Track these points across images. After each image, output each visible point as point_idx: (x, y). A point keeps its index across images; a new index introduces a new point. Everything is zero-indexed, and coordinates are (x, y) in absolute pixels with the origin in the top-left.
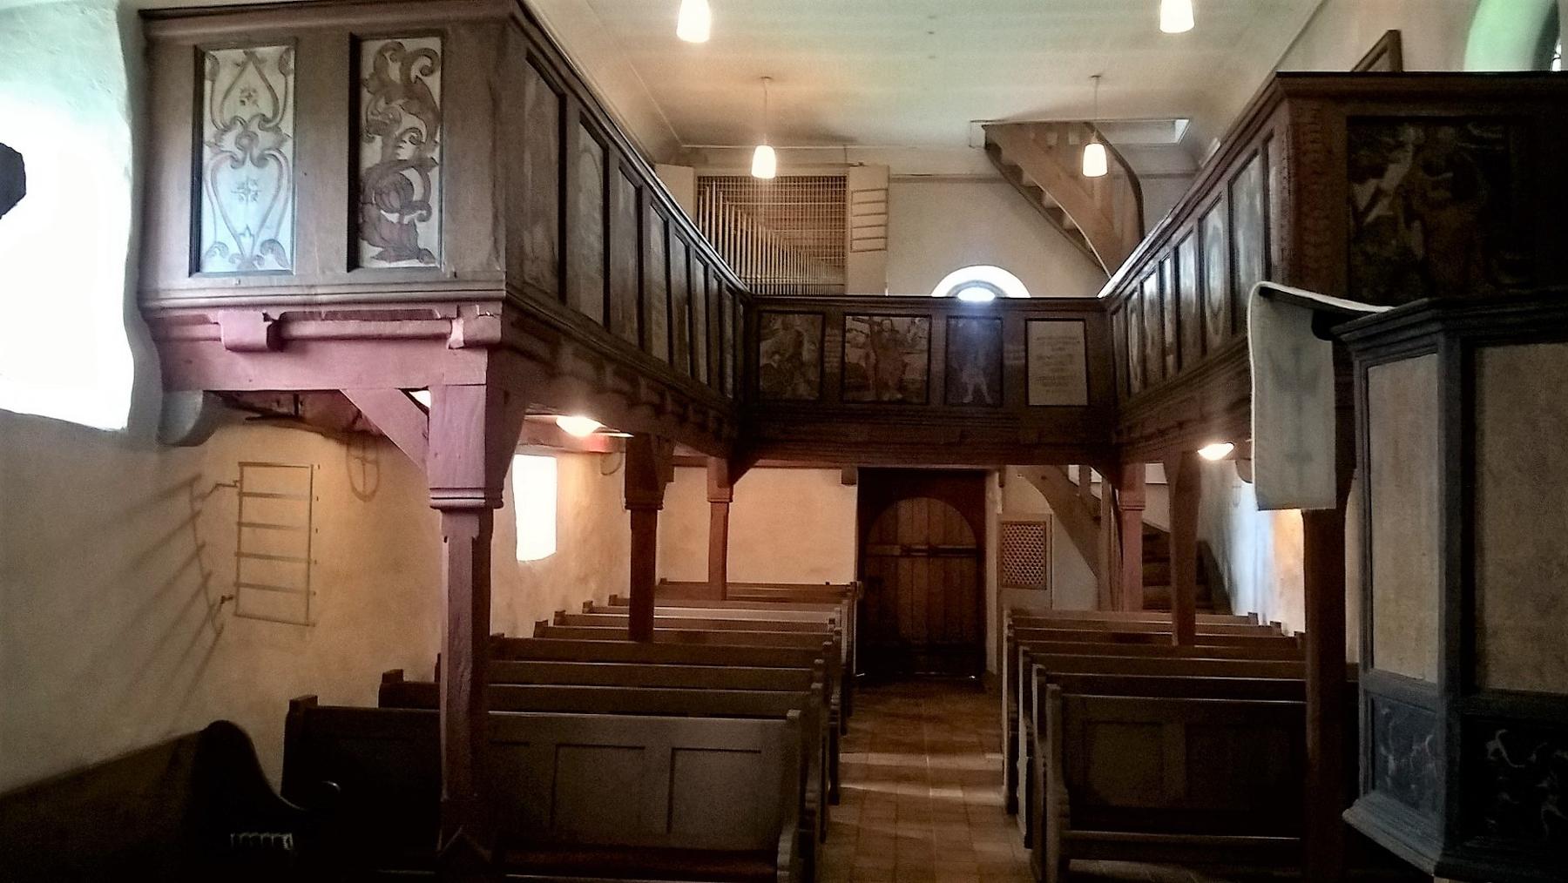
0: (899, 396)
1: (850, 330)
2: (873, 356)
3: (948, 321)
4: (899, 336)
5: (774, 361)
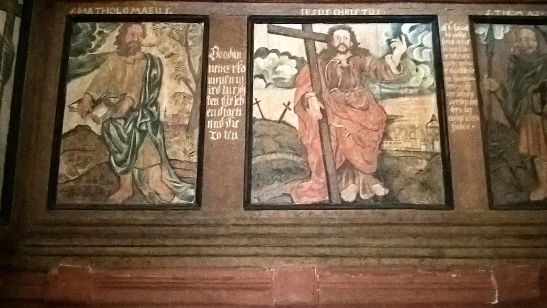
0: (380, 190)
1: (264, 52)
2: (315, 105)
3: (472, 30)
4: (368, 60)
5: (96, 120)
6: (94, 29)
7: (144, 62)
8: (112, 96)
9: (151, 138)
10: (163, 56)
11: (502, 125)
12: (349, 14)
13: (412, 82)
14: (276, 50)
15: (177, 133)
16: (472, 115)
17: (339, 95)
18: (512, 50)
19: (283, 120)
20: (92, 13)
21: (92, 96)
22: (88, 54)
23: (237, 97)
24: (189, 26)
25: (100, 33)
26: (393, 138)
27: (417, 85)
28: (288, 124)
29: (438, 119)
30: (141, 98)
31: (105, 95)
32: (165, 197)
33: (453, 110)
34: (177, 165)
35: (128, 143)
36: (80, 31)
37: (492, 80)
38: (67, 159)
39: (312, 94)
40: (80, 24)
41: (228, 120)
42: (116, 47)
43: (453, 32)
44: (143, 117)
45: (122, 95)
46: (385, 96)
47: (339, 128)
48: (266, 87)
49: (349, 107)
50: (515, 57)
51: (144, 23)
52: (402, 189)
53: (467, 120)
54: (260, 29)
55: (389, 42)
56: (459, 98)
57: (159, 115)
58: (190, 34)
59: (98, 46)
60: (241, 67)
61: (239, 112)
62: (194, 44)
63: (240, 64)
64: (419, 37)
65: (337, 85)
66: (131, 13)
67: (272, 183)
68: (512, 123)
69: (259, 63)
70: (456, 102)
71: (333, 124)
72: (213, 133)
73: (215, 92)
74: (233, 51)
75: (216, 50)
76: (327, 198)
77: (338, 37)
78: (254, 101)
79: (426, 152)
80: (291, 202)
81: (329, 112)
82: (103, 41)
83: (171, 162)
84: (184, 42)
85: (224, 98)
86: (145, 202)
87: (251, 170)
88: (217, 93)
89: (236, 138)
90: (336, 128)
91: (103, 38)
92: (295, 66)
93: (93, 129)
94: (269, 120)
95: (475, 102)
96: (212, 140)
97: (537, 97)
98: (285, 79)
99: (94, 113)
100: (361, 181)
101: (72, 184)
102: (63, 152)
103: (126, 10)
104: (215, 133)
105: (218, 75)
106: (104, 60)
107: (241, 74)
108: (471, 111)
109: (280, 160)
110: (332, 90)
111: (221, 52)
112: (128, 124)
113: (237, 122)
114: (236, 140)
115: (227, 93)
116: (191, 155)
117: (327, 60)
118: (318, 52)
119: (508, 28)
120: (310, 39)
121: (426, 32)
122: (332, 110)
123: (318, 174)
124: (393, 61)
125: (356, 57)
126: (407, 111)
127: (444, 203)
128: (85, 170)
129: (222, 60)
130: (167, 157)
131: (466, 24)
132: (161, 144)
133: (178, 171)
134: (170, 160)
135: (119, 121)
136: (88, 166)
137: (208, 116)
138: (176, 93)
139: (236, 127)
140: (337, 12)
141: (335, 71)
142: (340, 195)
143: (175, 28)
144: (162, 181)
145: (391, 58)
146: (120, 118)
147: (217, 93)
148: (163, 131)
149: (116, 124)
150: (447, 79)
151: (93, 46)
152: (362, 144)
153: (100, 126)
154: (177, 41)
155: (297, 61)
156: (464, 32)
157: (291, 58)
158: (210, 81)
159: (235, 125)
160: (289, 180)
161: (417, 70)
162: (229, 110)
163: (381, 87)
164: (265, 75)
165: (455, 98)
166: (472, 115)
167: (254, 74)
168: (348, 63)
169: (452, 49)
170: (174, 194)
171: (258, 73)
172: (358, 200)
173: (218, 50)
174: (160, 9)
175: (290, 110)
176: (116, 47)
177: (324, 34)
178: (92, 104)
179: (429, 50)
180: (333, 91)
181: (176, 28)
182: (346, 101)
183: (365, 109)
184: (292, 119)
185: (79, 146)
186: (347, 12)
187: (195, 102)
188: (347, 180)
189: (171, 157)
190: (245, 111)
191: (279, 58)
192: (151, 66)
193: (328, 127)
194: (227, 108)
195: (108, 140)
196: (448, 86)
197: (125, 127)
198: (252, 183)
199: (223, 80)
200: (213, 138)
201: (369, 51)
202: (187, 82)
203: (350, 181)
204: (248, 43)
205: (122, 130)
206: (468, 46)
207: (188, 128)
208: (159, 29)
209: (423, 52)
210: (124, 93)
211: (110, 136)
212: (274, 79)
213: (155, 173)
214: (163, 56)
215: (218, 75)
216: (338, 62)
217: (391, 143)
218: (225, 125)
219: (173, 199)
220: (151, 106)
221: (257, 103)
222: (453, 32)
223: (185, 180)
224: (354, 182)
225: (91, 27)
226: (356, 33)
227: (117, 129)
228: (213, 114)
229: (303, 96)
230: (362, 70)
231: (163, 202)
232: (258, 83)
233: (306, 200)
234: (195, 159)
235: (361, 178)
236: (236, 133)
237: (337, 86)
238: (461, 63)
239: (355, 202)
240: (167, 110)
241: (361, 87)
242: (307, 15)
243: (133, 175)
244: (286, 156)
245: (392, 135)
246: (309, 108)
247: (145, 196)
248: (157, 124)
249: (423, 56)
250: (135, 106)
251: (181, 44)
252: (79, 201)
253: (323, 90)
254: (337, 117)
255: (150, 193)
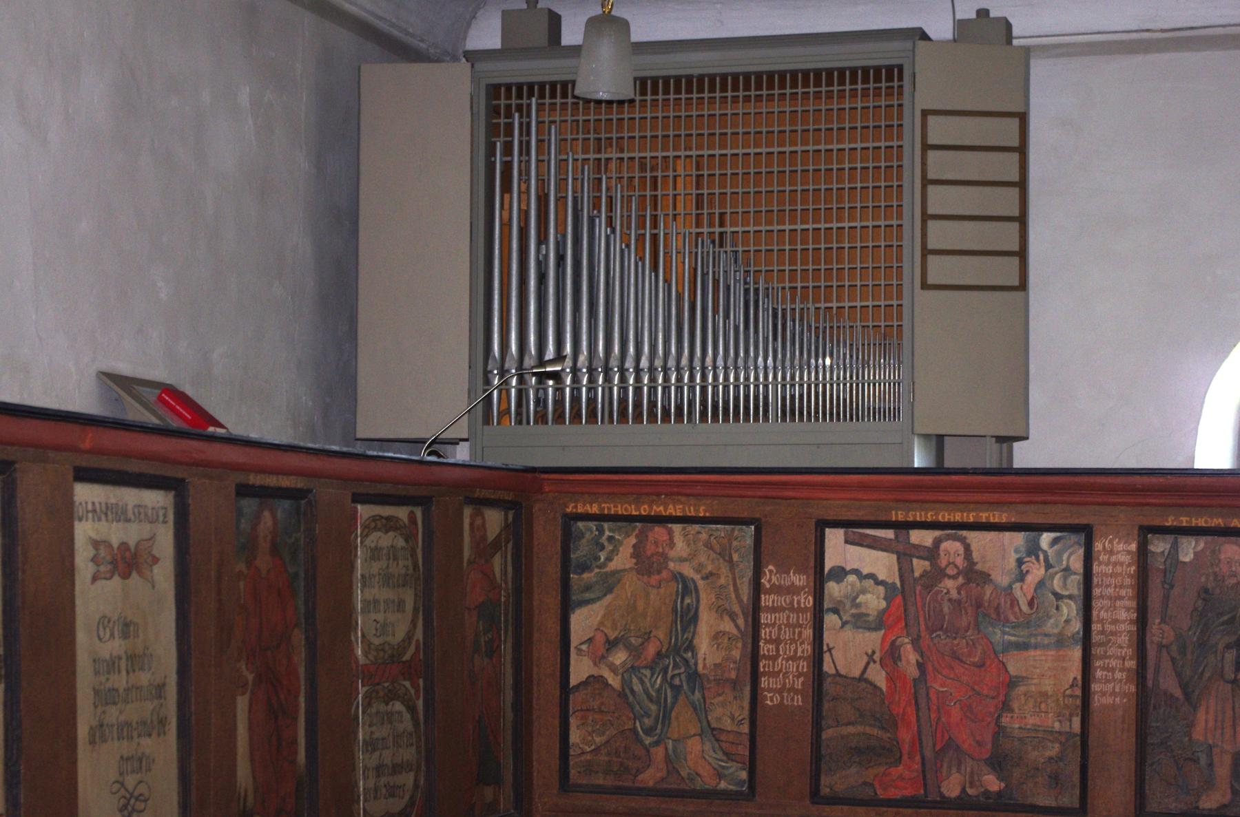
2: (910, 657)
5: (613, 669)
6: (601, 531)
7: (673, 586)
8: (632, 635)
9: (687, 697)
10: (699, 576)
11: (1172, 696)
12: (960, 521)
13: (1050, 627)
14: (857, 570)
15: (720, 692)
16: (1126, 683)
17: (943, 642)
18: (1203, 579)
19: (865, 676)
20: (597, 512)
21: (606, 635)
22: (597, 570)
23: (801, 644)
24: (733, 530)
25: (610, 539)
26: (1017, 711)
27: (1056, 631)
28: (871, 684)
29: (1080, 683)
30: (671, 639)
31: (622, 633)
32: (707, 781)
33: (1099, 673)
34: (723, 737)
35: (658, 703)
36: (582, 535)
37: (1166, 627)
38: (579, 723)
39: (906, 640)
40: (580, 524)
41: (788, 677)
42: (634, 561)
43: (1111, 552)
44: (676, 666)
45: (645, 633)
46: (1008, 647)
47: (942, 692)
48: (842, 627)
49: (957, 661)
50: (1206, 591)
51: (670, 525)
52: (1023, 783)
53: (1117, 690)
54: (834, 538)
55: (1020, 562)
56: (1110, 657)
57: (696, 664)
58: (735, 543)
59: (609, 559)
60: (805, 598)
61: (803, 667)
62: (741, 560)
63: (804, 594)
64: (1065, 557)
65: (943, 626)
66: (653, 514)
67: (850, 767)
68: (1187, 695)
69: (833, 589)
70: (1104, 664)
71: (934, 685)
72: (769, 695)
73: (770, 636)
74: (794, 573)
75: (771, 571)
76: (922, 792)
77: (947, 553)
78: (825, 648)
79: (1060, 733)
80: (873, 794)
81: (930, 668)
82: (615, 551)
83: (715, 733)
84: (725, 554)
85: (782, 645)
86: (683, 786)
87: (820, 747)
88: (774, 638)
89: (800, 703)
90: (938, 692)
91: (615, 546)
92: (882, 596)
93: (610, 681)
94: (846, 677)
95: (1131, 664)
96: (767, 704)
97: (1230, 656)
98: (868, 615)
99: (610, 659)
100: (968, 769)
101: (588, 757)
102: (573, 713)
103: (645, 508)
104: (771, 695)
105: (774, 610)
106: (619, 581)
107: (805, 610)
108: (1124, 677)
109: (859, 734)
110: (934, 635)
111: (778, 575)
112: (656, 676)
113: (801, 680)
114: (799, 706)
115: (787, 638)
116: (740, 723)
117: (928, 588)
118: (917, 574)
119: (1201, 543)
120: (905, 554)
121: (1077, 547)
122: (933, 666)
123: (911, 758)
124: (1022, 594)
125: (971, 584)
126: (1038, 671)
127: (1078, 806)
128: (604, 739)
129: (780, 587)
130: (709, 725)
131: (1135, 540)
132: (700, 705)
133: (723, 744)
134: (713, 729)
135: (643, 671)
136: (608, 733)
137: (762, 670)
138: (718, 633)
139: (800, 687)
140: (943, 517)
141: (940, 605)
142: (939, 787)
143: (714, 533)
144: (704, 758)
145: (1021, 588)
146: (646, 667)
147: (774, 638)
148: (703, 688)
149: (640, 675)
150: (1096, 627)
151: (602, 559)
152: (973, 717)
153: (620, 677)
154: (716, 553)
155: (886, 588)
156: (1129, 552)
157: (878, 583)
158: (765, 618)
159: (799, 684)
160: (872, 764)
161: (1058, 608)
162: (790, 662)
163: (1004, 633)
164: (841, 608)
165: (1105, 657)
166: (1126, 683)
167: (826, 606)
168: (959, 593)
169: (1107, 581)
170: (720, 776)
171: (831, 606)
172: (963, 795)
173: (775, 571)
174: (692, 508)
175: (875, 662)
176: (634, 561)
177: (926, 547)
178: (607, 647)
179: (1078, 577)
180: (936, 636)
181: (716, 534)
182: (954, 652)
183: (981, 665)
184: (878, 676)
185: (595, 704)
186: (957, 517)
187: (744, 646)
188: (950, 767)
189: (714, 725)
190: (812, 664)
191: (861, 582)
192: (683, 592)
193: (927, 689)
194: (787, 660)
195: (631, 698)
196: (1096, 638)
197: (653, 680)
198: (823, 766)
199: (782, 617)
200: (768, 702)
201: (990, 575)
202: (733, 616)
203: (954, 770)
204: (816, 561)
205: (648, 684)
206: (1130, 576)
207: (735, 684)
208: (691, 536)
209: (1069, 581)
210: (648, 631)
211: (632, 691)
212: (853, 616)
213: (694, 746)
214: (699, 576)
215: (774, 610)
216: (945, 591)
217: (1012, 717)
218: (785, 684)
219: (719, 783)
220: (686, 650)
221: (830, 650)
222: (1111, 552)
223: (734, 757)
224: (959, 771)
225: (597, 529)
226: (973, 548)
227: (642, 682)
228: (769, 668)
229: (893, 642)
230: (979, 605)
231: (706, 787)
232: (830, 620)
233: (895, 793)
234: (745, 729)
235: (969, 764)
236: (799, 697)
237: (941, 629)
238: (1118, 603)
239: (958, 797)
240: (707, 656)
241: (976, 632)
242: (900, 519)
243: (666, 749)
244: (868, 730)
245: (1015, 706)
246: (901, 660)
247: (683, 778)
248: (694, 677)
249: (1068, 586)
250: (664, 650)
251: (724, 560)
252: (600, 780)
253: (923, 634)
254: (940, 676)
255: (689, 774)
